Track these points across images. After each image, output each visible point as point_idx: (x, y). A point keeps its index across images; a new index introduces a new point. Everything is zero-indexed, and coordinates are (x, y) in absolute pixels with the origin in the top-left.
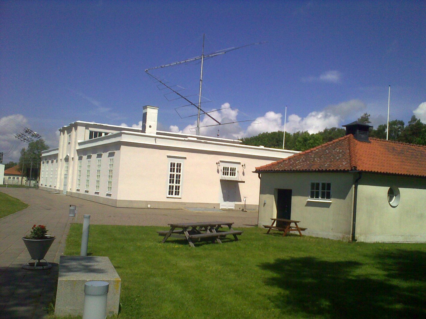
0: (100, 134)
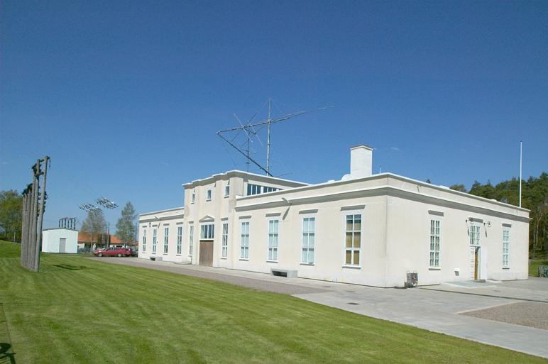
0: (259, 187)
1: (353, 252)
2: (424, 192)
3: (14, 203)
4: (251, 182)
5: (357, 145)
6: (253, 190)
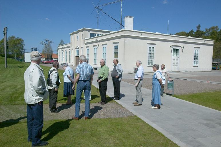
0: (95, 34)
1: (151, 60)
2: (144, 36)
3: (15, 42)
4: (91, 32)
5: (127, 16)
6: (92, 35)
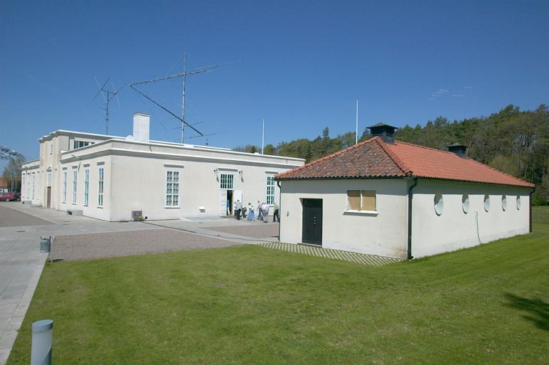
4: (77, 139)
